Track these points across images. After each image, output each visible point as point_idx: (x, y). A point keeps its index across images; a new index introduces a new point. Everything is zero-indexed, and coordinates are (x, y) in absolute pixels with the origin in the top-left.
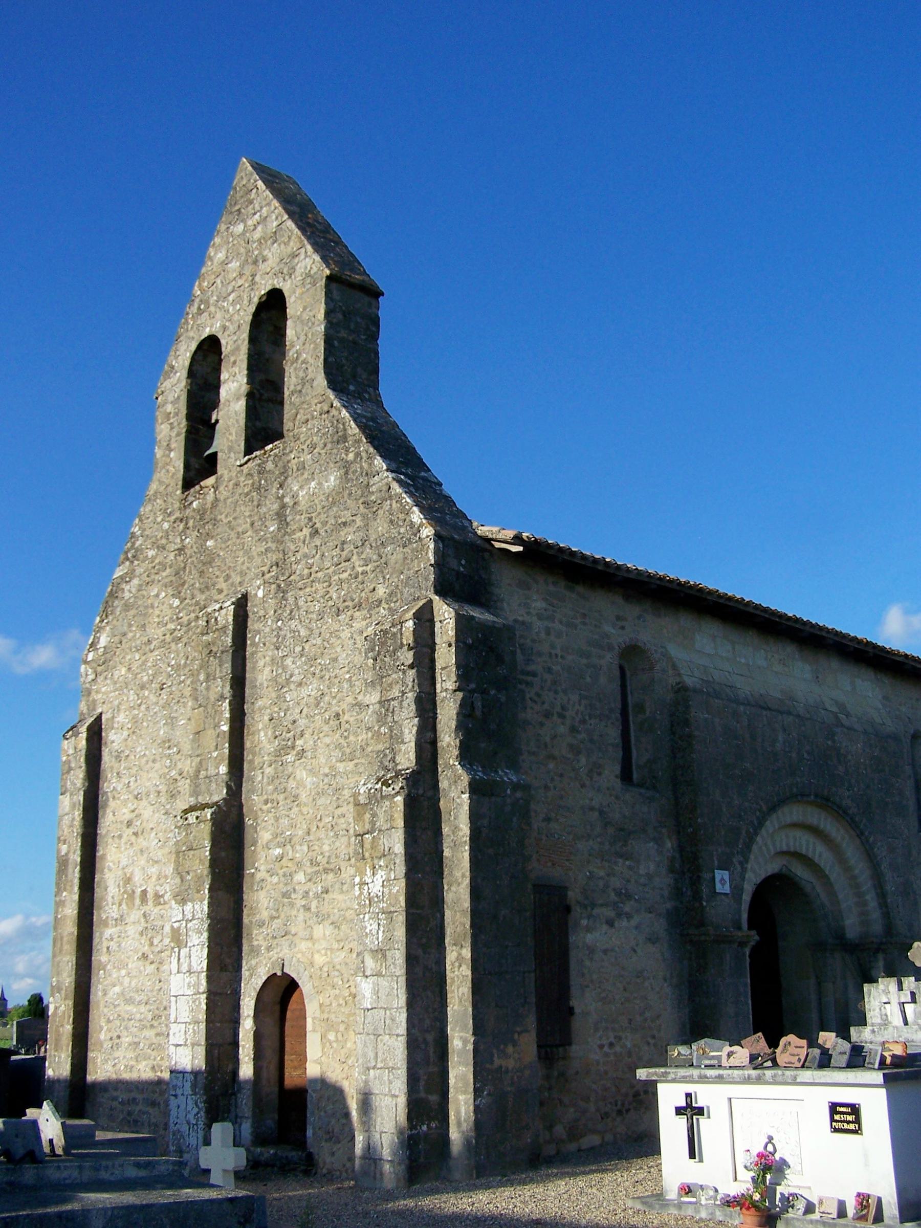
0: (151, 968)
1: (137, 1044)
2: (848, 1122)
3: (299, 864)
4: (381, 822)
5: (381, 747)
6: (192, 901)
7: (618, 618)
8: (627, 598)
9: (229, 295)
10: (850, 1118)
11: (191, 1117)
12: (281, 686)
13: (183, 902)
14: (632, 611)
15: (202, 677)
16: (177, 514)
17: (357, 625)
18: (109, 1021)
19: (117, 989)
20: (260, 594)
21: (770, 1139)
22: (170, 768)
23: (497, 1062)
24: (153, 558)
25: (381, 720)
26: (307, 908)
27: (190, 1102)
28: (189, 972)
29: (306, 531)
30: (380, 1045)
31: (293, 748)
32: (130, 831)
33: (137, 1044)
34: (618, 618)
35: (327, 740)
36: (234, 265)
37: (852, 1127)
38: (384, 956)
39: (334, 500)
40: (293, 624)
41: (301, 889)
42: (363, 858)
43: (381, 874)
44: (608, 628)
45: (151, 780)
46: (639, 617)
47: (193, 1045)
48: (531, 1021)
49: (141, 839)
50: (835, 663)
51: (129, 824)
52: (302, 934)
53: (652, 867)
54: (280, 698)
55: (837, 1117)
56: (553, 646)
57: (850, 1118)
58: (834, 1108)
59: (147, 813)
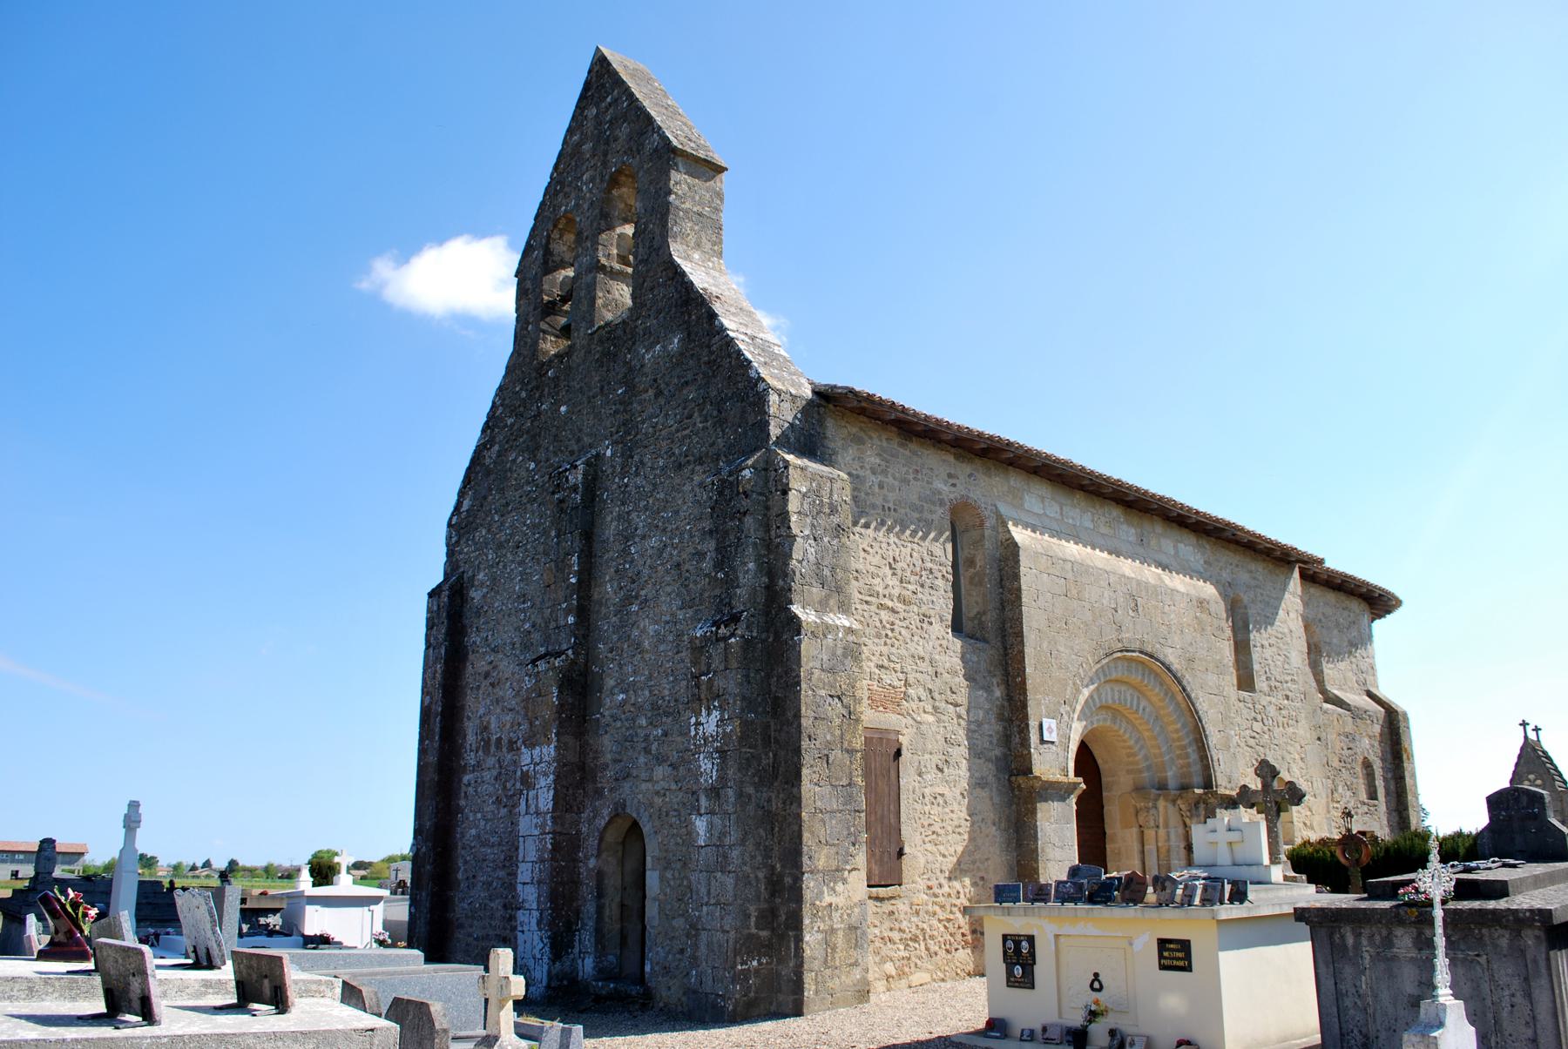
0: (504, 811)
1: (490, 884)
2: (1178, 959)
3: (640, 708)
4: (716, 663)
5: (717, 592)
6: (540, 745)
7: (950, 476)
8: (957, 457)
9: (609, 823)
10: (1180, 955)
11: (536, 951)
12: (627, 537)
13: (532, 746)
14: (964, 469)
15: (553, 533)
16: (534, 383)
17: (697, 478)
18: (466, 862)
19: (473, 832)
20: (609, 453)
21: (1096, 975)
22: (524, 621)
23: (827, 899)
24: (513, 425)
25: (719, 565)
26: (647, 751)
27: (536, 938)
28: (538, 813)
29: (651, 393)
30: (713, 882)
31: (636, 597)
32: (487, 683)
33: (490, 884)
34: (950, 476)
35: (669, 589)
36: (587, 147)
37: (1181, 963)
38: (718, 795)
39: (680, 359)
40: (638, 481)
41: (642, 733)
42: (700, 699)
43: (716, 714)
44: (938, 485)
45: (507, 634)
46: (970, 476)
47: (539, 882)
48: (861, 859)
49: (497, 690)
50: (1159, 528)
51: (487, 675)
52: (643, 775)
53: (981, 713)
54: (625, 552)
55: (1166, 954)
56: (885, 500)
57: (1180, 955)
58: (1163, 943)
59: (503, 665)
